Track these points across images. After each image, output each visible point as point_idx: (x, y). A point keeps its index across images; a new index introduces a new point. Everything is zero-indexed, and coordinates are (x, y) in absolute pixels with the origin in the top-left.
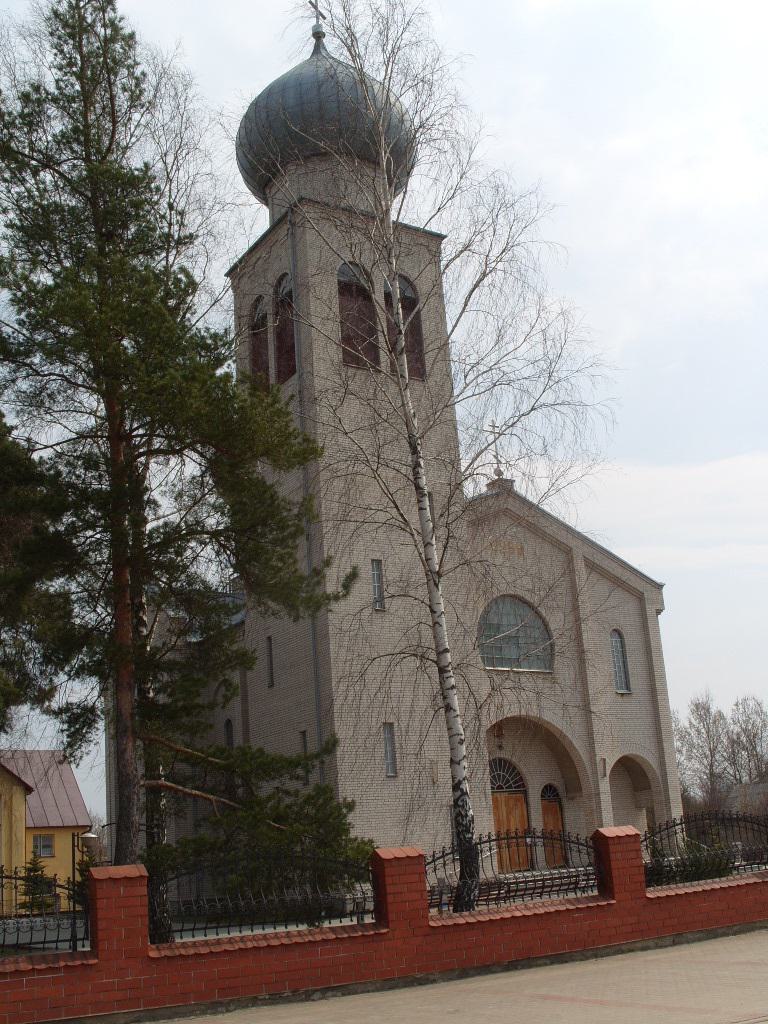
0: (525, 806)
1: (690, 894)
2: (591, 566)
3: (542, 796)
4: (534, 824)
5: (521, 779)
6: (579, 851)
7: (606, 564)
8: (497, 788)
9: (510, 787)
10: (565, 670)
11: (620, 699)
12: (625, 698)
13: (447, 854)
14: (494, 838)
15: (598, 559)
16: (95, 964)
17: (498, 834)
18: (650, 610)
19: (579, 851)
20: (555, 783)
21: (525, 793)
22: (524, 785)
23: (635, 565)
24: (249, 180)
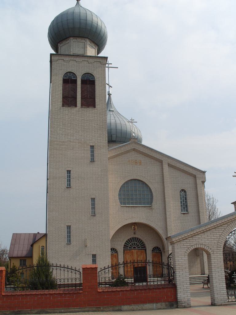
0: (145, 254)
1: (52, 313)
2: (169, 165)
3: (152, 251)
4: (163, 261)
5: (144, 245)
6: (72, 272)
7: (178, 165)
8: (35, 235)
9: (139, 247)
10: (157, 203)
11: (183, 215)
12: (185, 215)
13: (106, 269)
14: (110, 266)
15: (173, 163)
16: (82, 293)
17: (112, 265)
18: (199, 182)
19: (72, 272)
20: (159, 246)
21: (146, 250)
22: (145, 247)
23: (50, 57)
24: (53, 47)
